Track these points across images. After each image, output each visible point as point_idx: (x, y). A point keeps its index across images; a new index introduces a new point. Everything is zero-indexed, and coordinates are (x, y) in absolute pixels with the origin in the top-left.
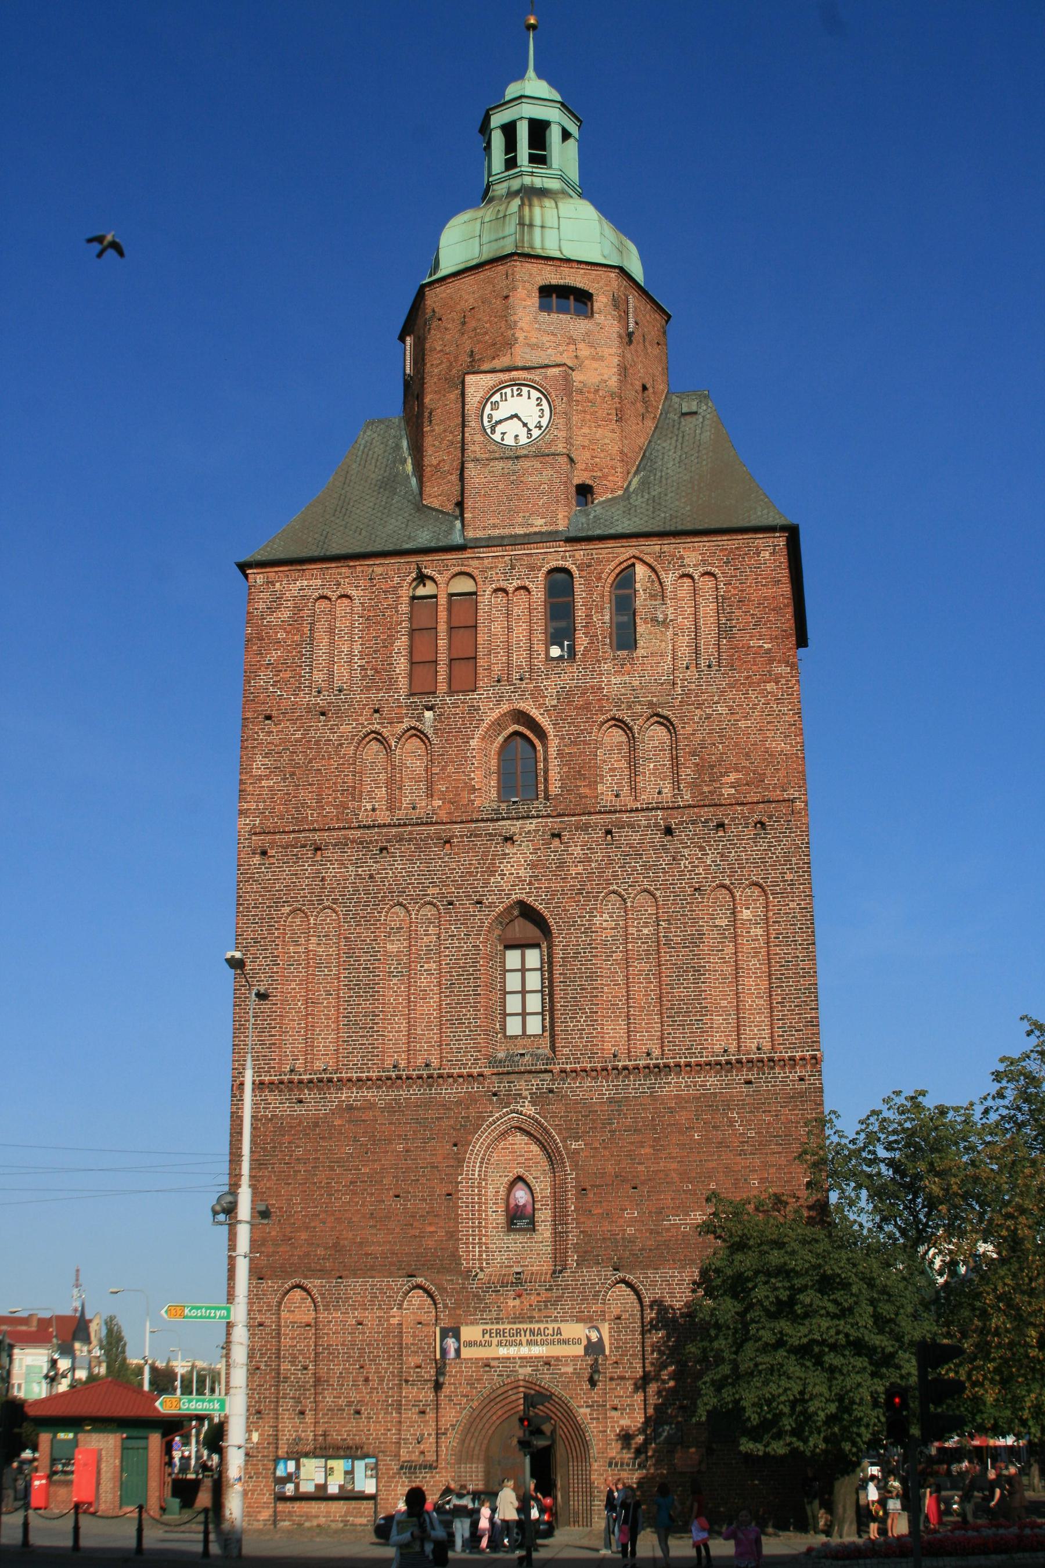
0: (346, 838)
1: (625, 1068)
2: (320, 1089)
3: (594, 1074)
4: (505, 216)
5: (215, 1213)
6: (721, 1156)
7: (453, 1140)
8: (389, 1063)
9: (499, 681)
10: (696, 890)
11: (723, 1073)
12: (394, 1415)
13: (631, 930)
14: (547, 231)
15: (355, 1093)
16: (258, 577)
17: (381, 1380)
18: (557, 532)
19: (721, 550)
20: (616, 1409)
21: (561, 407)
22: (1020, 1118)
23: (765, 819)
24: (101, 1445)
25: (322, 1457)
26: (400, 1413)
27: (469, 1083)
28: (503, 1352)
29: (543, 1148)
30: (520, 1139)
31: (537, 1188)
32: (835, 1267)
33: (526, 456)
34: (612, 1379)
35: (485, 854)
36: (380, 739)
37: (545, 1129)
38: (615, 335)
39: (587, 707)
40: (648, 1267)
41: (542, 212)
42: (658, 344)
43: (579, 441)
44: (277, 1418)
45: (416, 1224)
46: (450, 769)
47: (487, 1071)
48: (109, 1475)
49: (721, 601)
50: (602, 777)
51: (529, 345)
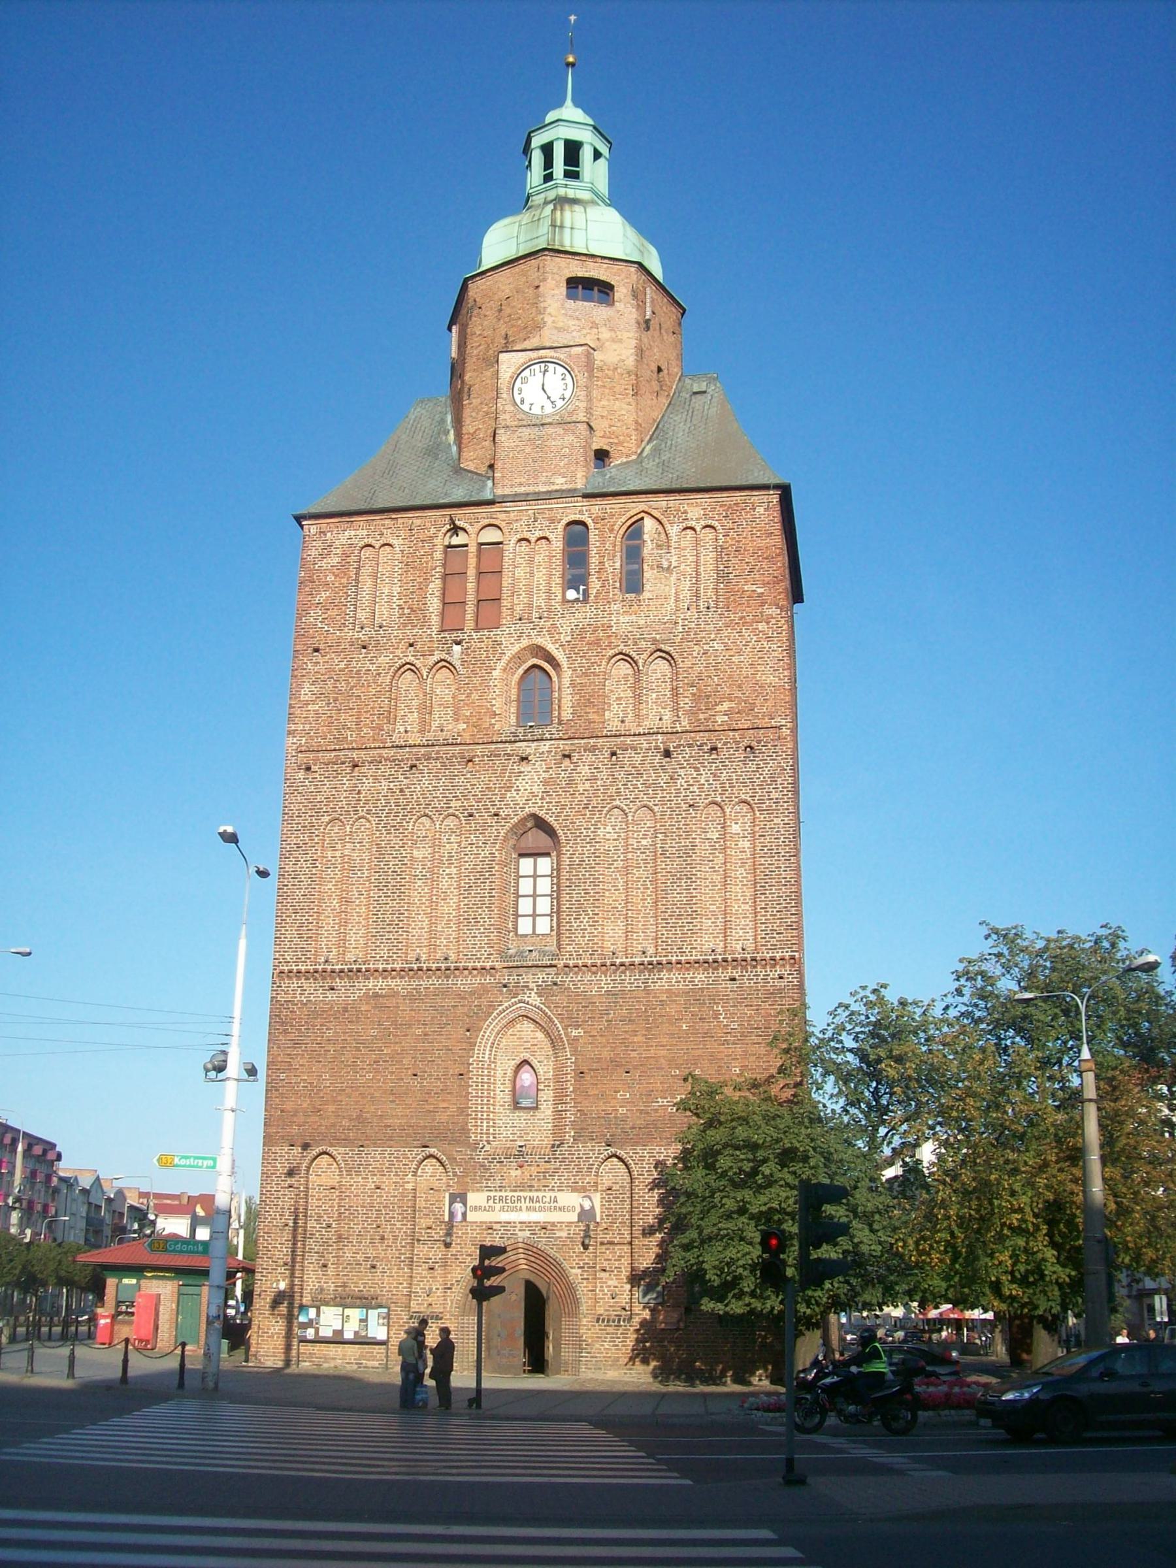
0: (381, 756)
1: (622, 965)
2: (350, 978)
3: (594, 969)
4: (539, 219)
5: (207, 1070)
6: (705, 1045)
7: (467, 1026)
8: (412, 956)
9: (520, 619)
10: (690, 806)
11: (711, 971)
12: (406, 1270)
13: (631, 841)
14: (575, 231)
15: (381, 983)
16: (311, 527)
17: (396, 1238)
18: (575, 490)
19: (721, 506)
20: (604, 1270)
21: (582, 380)
22: (978, 1014)
23: (754, 744)
24: (160, 1291)
25: (341, 1306)
26: (411, 1269)
27: (483, 975)
28: (505, 1217)
29: (548, 1035)
30: (528, 1026)
31: (541, 1071)
32: (794, 1141)
33: (550, 424)
34: (602, 1244)
35: (504, 771)
36: (412, 668)
37: (549, 1017)
38: (633, 321)
39: (597, 643)
40: (636, 1144)
41: (570, 216)
42: (674, 333)
43: (597, 412)
44: (302, 1270)
45: (430, 1100)
46: (475, 696)
47: (497, 965)
48: (167, 1317)
49: (720, 551)
50: (610, 705)
51: (556, 328)
